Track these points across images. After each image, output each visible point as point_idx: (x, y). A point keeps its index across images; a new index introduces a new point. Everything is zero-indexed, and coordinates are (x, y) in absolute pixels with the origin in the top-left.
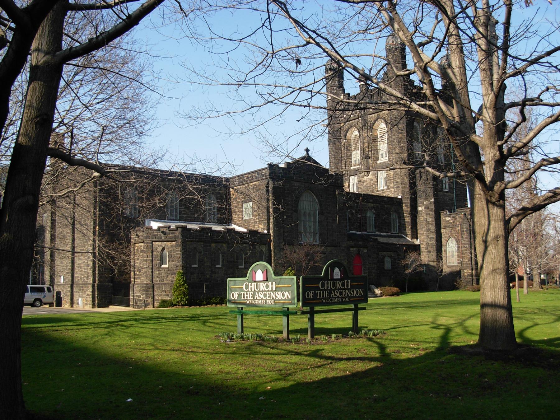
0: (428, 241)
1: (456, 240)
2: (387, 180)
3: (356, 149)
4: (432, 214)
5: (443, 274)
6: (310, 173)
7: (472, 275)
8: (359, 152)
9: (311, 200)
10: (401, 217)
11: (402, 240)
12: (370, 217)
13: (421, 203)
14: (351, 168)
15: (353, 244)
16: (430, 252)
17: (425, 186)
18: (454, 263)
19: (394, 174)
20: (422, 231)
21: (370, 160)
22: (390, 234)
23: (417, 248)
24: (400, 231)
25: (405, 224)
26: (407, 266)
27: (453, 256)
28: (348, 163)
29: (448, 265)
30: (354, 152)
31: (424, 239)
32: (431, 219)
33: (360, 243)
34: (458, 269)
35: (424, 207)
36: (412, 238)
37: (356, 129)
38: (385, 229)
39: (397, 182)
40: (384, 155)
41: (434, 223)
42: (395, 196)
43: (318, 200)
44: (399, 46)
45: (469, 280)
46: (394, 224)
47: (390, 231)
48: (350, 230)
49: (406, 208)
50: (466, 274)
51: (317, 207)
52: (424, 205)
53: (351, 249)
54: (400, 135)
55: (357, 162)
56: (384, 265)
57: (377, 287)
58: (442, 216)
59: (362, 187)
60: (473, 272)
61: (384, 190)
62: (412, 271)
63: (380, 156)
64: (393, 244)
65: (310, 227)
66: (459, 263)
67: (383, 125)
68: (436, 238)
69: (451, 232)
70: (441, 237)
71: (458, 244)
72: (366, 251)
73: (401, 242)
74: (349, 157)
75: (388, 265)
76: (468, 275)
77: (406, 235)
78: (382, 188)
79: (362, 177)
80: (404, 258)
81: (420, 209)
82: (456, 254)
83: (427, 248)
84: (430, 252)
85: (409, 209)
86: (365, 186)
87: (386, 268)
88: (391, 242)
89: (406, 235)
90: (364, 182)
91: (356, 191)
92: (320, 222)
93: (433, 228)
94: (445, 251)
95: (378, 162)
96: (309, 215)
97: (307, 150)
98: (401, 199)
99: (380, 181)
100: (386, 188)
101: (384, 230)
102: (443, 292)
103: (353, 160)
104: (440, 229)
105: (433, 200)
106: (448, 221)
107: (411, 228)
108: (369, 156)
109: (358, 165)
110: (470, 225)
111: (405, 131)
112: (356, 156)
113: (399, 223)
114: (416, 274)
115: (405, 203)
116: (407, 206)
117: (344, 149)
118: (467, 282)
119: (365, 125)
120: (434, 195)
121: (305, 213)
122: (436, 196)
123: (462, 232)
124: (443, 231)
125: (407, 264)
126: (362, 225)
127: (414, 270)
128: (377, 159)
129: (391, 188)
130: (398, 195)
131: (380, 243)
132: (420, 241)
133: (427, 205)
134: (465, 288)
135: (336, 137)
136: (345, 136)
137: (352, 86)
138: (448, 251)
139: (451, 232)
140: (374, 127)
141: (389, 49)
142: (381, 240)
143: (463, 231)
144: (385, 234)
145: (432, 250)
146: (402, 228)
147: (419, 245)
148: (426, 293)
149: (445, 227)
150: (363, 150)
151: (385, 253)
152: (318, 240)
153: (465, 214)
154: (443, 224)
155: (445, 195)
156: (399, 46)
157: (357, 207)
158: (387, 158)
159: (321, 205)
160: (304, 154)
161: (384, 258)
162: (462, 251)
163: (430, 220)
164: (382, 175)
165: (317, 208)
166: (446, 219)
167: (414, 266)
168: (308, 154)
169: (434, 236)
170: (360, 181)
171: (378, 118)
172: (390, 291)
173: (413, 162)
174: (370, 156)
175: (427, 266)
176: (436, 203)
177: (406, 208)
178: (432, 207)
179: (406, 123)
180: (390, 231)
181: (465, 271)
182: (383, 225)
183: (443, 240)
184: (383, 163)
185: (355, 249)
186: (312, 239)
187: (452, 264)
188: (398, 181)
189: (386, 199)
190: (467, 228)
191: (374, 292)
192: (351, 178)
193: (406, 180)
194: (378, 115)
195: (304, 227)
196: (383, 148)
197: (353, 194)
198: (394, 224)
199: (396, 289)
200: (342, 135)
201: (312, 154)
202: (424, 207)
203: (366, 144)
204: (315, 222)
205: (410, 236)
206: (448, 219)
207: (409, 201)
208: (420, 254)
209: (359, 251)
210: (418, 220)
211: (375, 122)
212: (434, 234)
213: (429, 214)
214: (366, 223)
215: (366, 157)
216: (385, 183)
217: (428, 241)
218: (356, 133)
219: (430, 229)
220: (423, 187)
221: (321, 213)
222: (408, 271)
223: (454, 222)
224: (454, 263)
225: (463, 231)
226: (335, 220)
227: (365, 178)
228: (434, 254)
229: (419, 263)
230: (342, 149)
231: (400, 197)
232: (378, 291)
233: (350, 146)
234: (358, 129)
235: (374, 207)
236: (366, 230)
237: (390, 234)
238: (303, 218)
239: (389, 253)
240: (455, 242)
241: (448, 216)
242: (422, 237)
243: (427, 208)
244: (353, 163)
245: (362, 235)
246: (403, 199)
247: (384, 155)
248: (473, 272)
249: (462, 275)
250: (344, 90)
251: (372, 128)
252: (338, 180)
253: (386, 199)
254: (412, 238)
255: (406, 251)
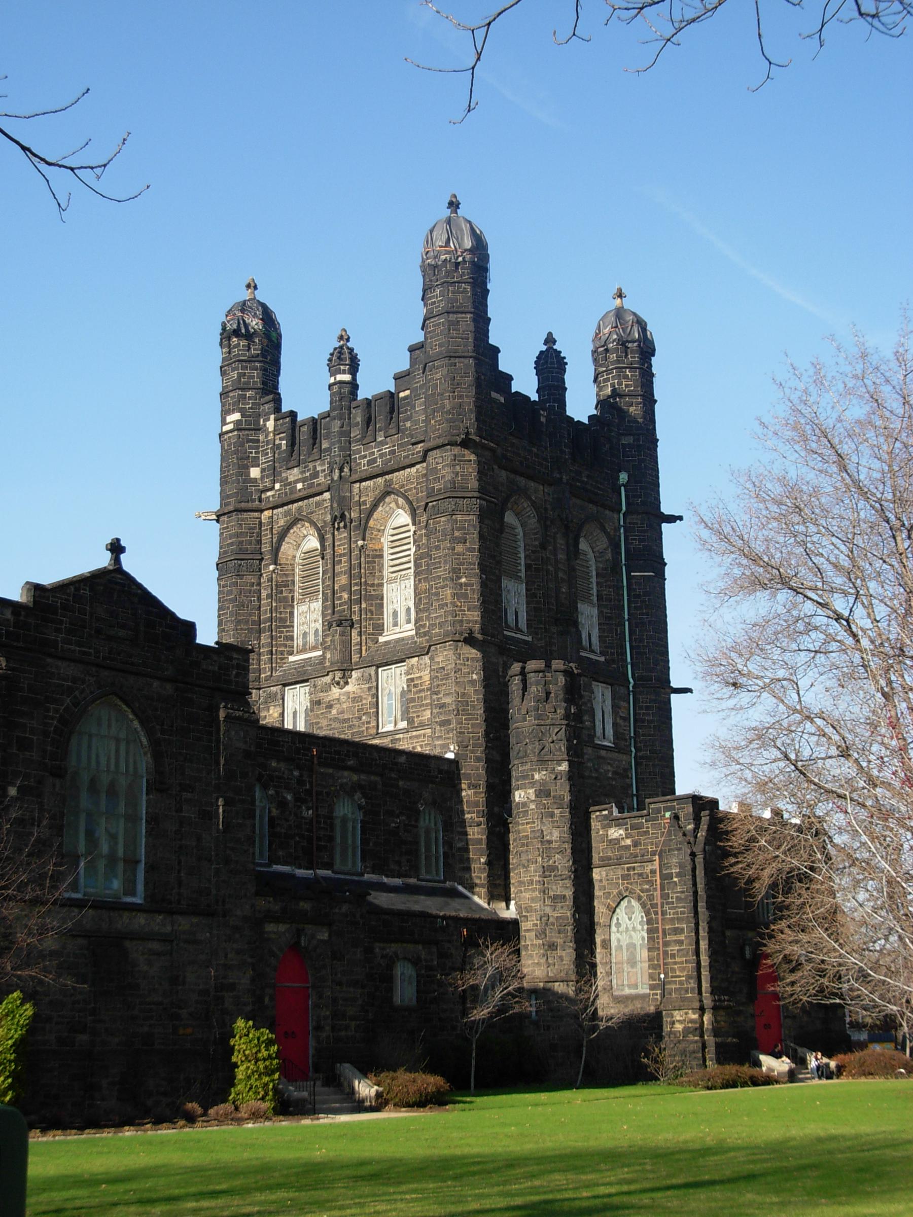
0: (548, 910)
1: (643, 905)
2: (409, 703)
3: (309, 594)
4: (562, 814)
5: (602, 1025)
6: (122, 633)
7: (700, 1031)
8: (317, 605)
9: (122, 735)
10: (454, 823)
11: (456, 903)
12: (344, 820)
13: (525, 777)
14: (292, 659)
15: (276, 908)
16: (552, 946)
17: (538, 717)
18: (636, 986)
19: (432, 679)
20: (524, 875)
21: (354, 633)
22: (413, 881)
23: (508, 932)
24: (450, 873)
25: (467, 850)
26: (474, 995)
27: (632, 963)
28: (281, 641)
29: (616, 993)
30: (303, 608)
31: (531, 901)
32: (557, 833)
33: (305, 905)
34: (652, 1009)
35: (536, 794)
36: (491, 898)
37: (312, 531)
38: (399, 863)
39: (443, 706)
40: (402, 617)
41: (568, 846)
42: (437, 752)
43: (150, 733)
44: (468, 257)
45: (692, 1047)
46: (428, 849)
47: (414, 870)
48: (273, 860)
49: (472, 795)
50: (679, 1027)
51: (145, 763)
52: (532, 785)
53: (270, 927)
54: (459, 548)
55: (311, 639)
56: (390, 990)
57: (364, 1072)
58: (595, 824)
59: (324, 723)
60: (706, 1018)
61: (397, 732)
62: (492, 1015)
63: (387, 619)
64: (424, 915)
65: (113, 837)
66: (652, 987)
67: (403, 518)
68: (576, 899)
69: (624, 877)
70: (591, 897)
71: (649, 922)
72: (324, 935)
73: (455, 909)
74: (286, 623)
75: (404, 990)
76: (686, 1031)
77: (471, 887)
78: (390, 727)
79: (327, 688)
80: (464, 966)
81: (518, 796)
82: (645, 954)
83: (542, 934)
84: (552, 946)
85: (482, 798)
86: (335, 719)
87: (397, 1000)
88: (417, 908)
89: (471, 887)
90: (330, 706)
91: (301, 727)
92: (153, 820)
93: (563, 862)
94: (606, 944)
95: (382, 639)
96: (112, 791)
97: (116, 548)
98: (455, 763)
99: (384, 702)
100: (403, 725)
101: (393, 866)
102: (596, 1090)
103: (297, 632)
104: (589, 869)
105: (564, 767)
106: (617, 841)
107: (489, 863)
108: (356, 612)
109: (314, 648)
110: (693, 855)
111: (476, 536)
112: (308, 618)
113: (448, 843)
114: (507, 1022)
115: (468, 777)
116: (475, 786)
117: (270, 596)
118: (683, 1052)
119: (343, 517)
120: (569, 749)
121: (93, 782)
122: (575, 755)
123: (666, 877)
124: (596, 874)
125: (474, 988)
126: (315, 845)
127: (502, 1009)
128: (379, 629)
129: (422, 725)
130: (446, 747)
131: (378, 911)
132: (519, 907)
133: (543, 783)
134: (677, 1077)
135: (245, 561)
136: (276, 551)
137: (305, 389)
138: (614, 944)
139: (624, 877)
140: (371, 523)
141: (435, 267)
142: (382, 899)
143: (670, 876)
144: (397, 881)
145: (560, 941)
146: (456, 862)
147: (515, 923)
148: (543, 1097)
149: (606, 863)
150: (331, 598)
151: (393, 948)
152: (140, 887)
153: (676, 817)
154: (599, 850)
155: (599, 757)
156: (468, 257)
157: (300, 782)
158: (411, 626)
159: (157, 756)
160: (103, 560)
161: (391, 963)
162: (666, 944)
163: (556, 835)
164: (392, 680)
165: (142, 768)
166: (610, 832)
167: (498, 995)
168: (117, 560)
169: (569, 893)
170: (319, 703)
171: (388, 493)
172: (412, 1089)
173: (496, 647)
174: (355, 618)
175: (541, 994)
176: (575, 776)
177: (472, 795)
178: (563, 791)
179: (481, 509)
180: (414, 870)
181: (678, 1015)
182: (391, 849)
183: (600, 908)
184: (398, 641)
185: (282, 928)
186: (116, 884)
187: (627, 991)
188: (448, 700)
189: (402, 759)
190: (681, 866)
191: (352, 1091)
192: (289, 692)
193: (474, 697)
194: (388, 483)
195: (90, 833)
196: (399, 596)
197: (294, 735)
198: (428, 849)
199: (432, 1082)
200: (266, 548)
201: (128, 563)
202: (536, 794)
203: (343, 580)
204: (132, 819)
205: (483, 891)
206: (615, 833)
207: (482, 772)
208: (518, 952)
209: (299, 933)
210: (512, 837)
211: (375, 506)
212: (569, 883)
213: (552, 815)
214: (331, 839)
215: (339, 622)
216: (403, 702)
217: (548, 910)
218: (313, 543)
219: (553, 868)
220: (531, 720)
221: (157, 786)
222: (480, 1013)
223: (636, 844)
224: (636, 986)
225: (670, 876)
226: (208, 815)
227: (336, 691)
228: (567, 955)
229: (516, 985)
230: (264, 594)
231: (450, 756)
232: (366, 1089)
233: (288, 584)
234: (319, 530)
235: (358, 787)
236: (329, 866)
237: (413, 881)
238: (85, 801)
239: (410, 947)
240: (639, 915)
241: (618, 822)
242: (527, 895)
243: (544, 792)
244: (298, 642)
245: (317, 880)
246: (462, 763)
247: (402, 617)
248: (706, 1018)
249: (667, 1029)
250: (278, 401)
251: (363, 528)
252: (226, 673)
253: (402, 759)
254: (491, 898)
255: (471, 943)
